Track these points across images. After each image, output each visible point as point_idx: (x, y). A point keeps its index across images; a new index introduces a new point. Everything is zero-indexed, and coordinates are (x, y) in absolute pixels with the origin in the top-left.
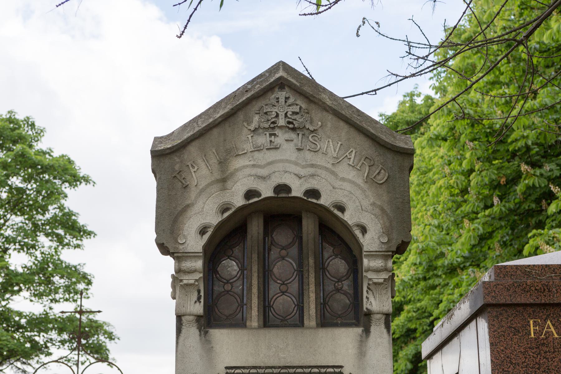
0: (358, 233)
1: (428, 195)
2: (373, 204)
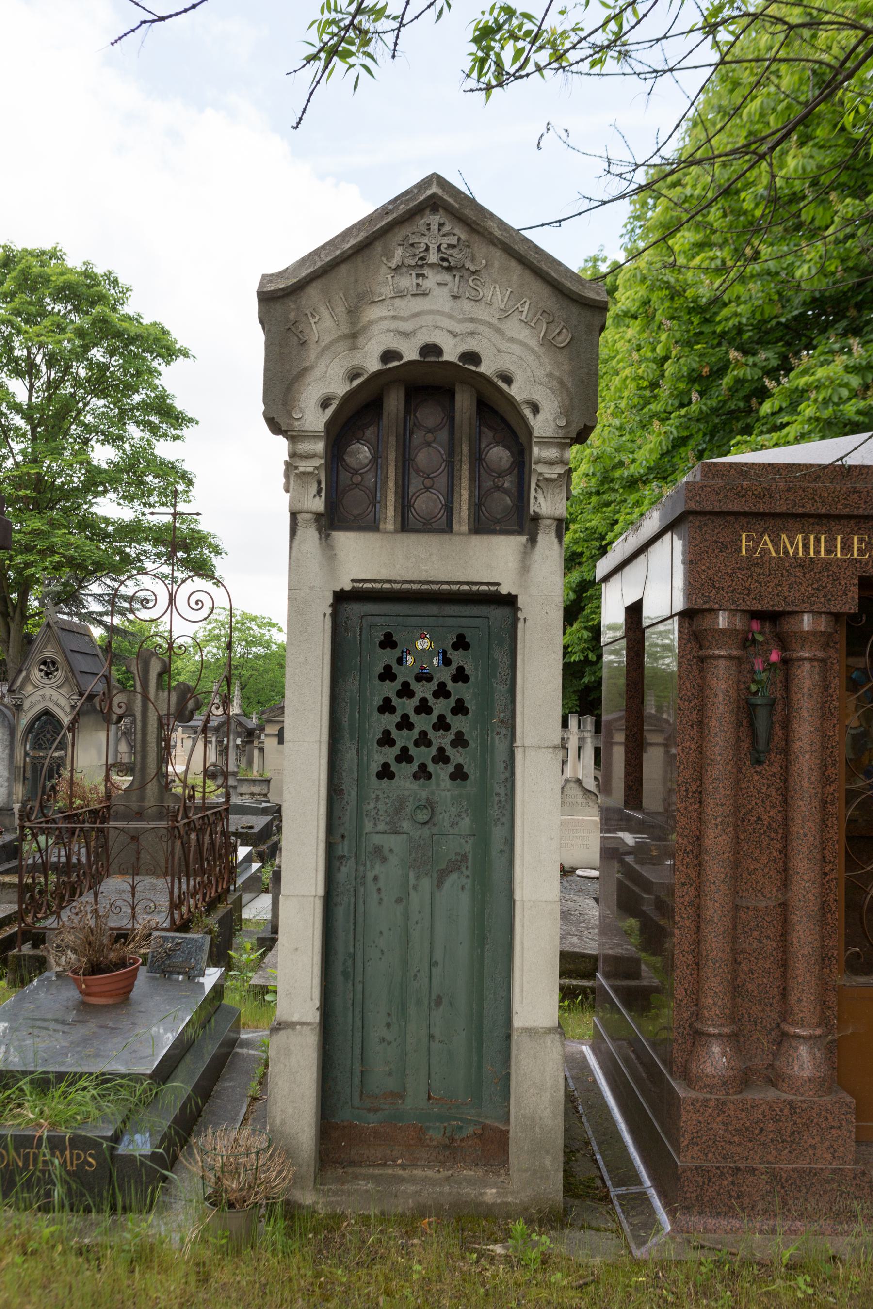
0: (527, 412)
1: (609, 389)
2: (550, 375)
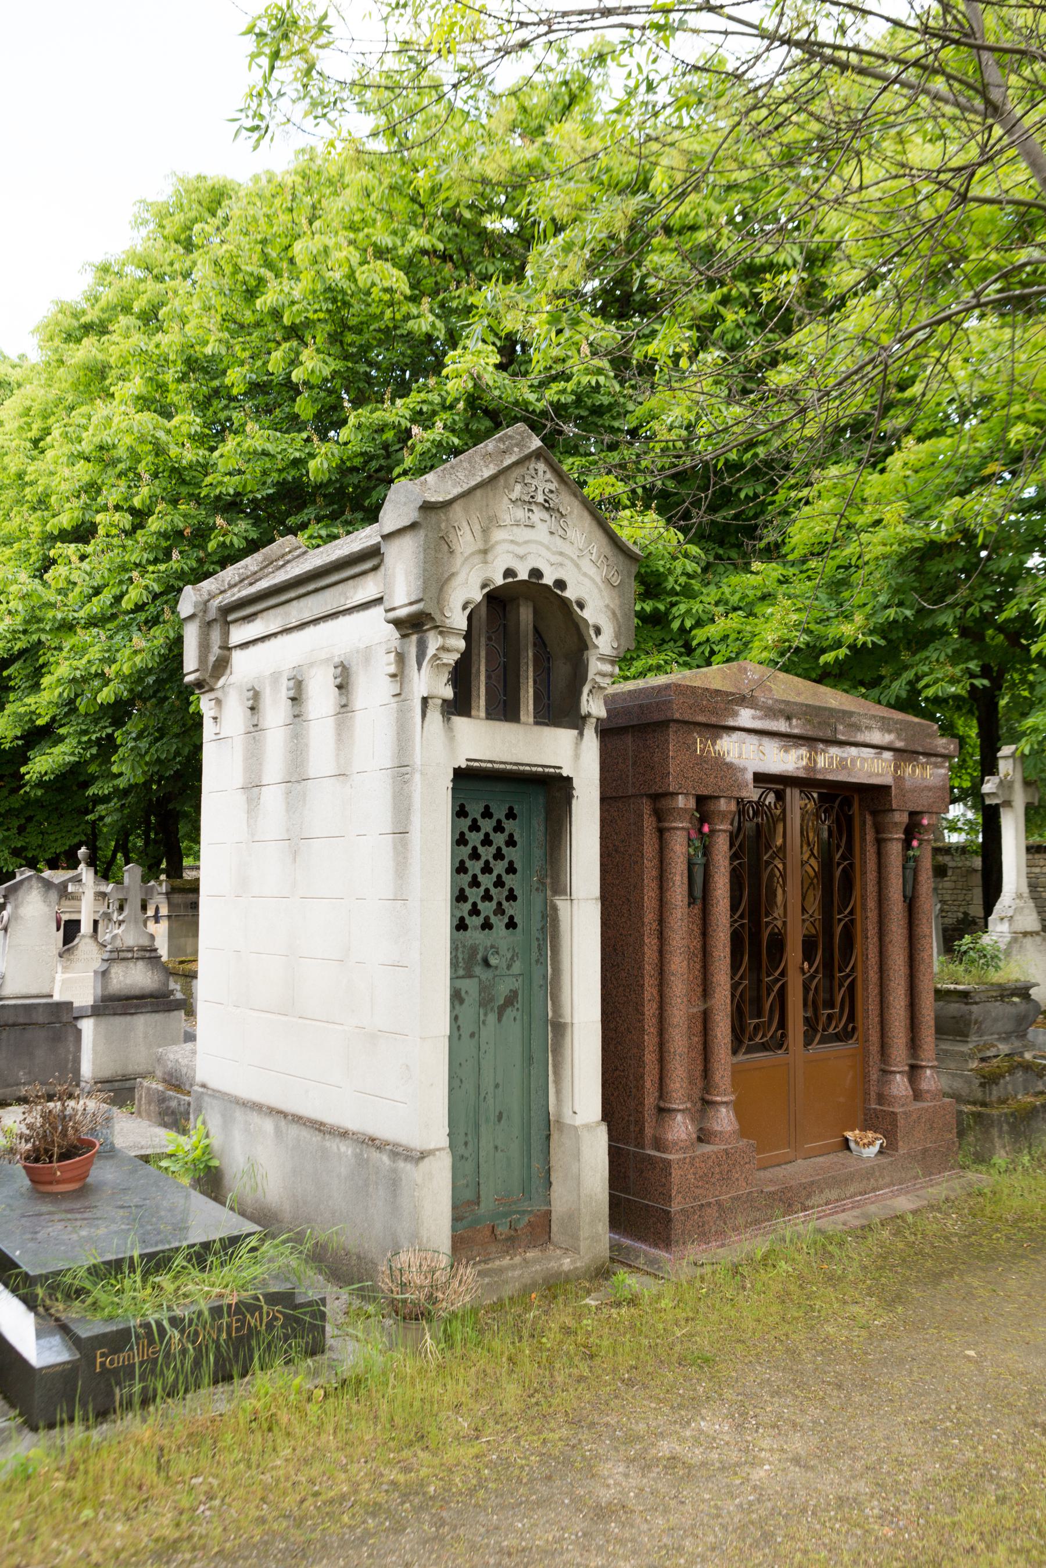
2: (607, 606)
